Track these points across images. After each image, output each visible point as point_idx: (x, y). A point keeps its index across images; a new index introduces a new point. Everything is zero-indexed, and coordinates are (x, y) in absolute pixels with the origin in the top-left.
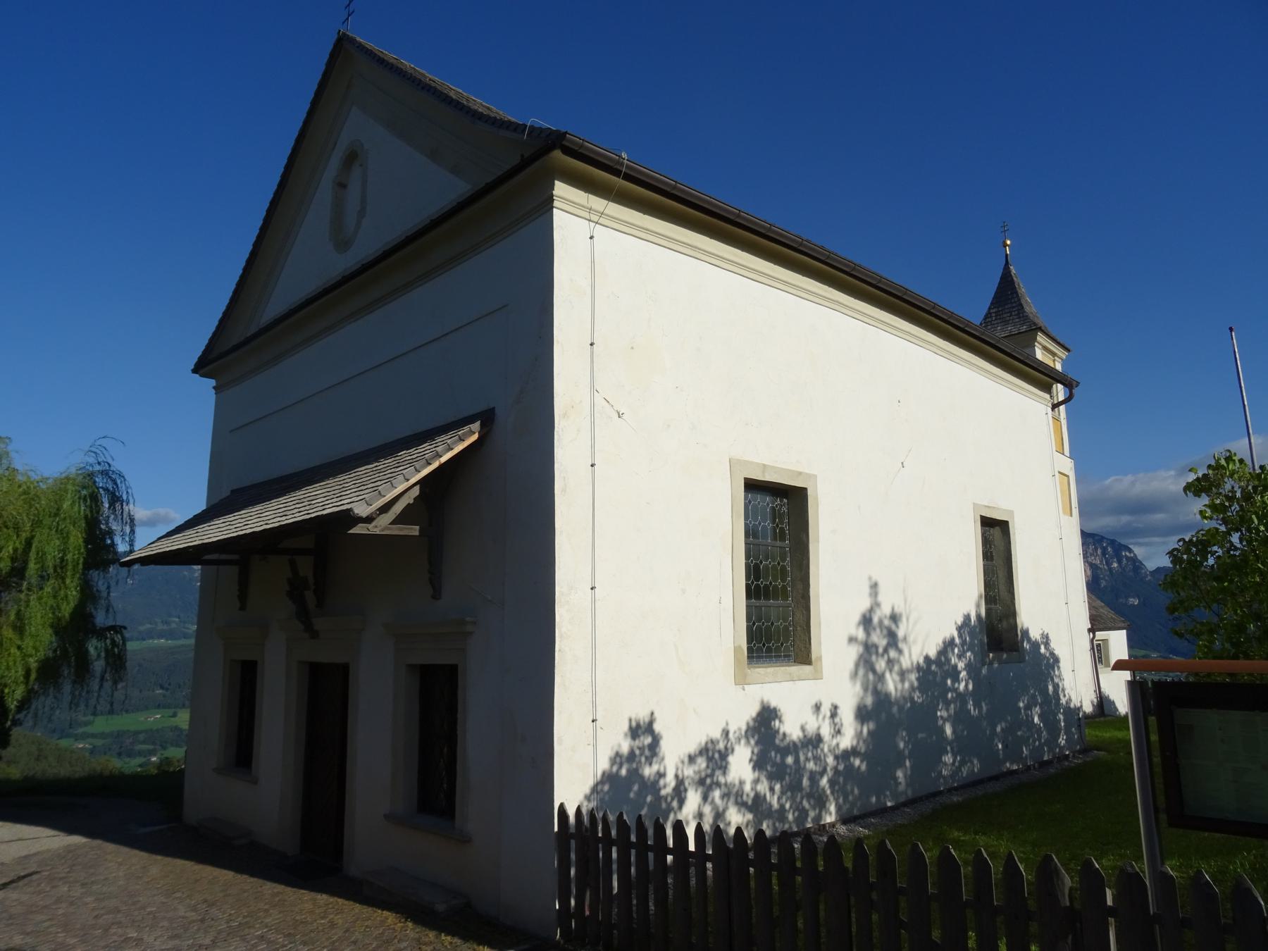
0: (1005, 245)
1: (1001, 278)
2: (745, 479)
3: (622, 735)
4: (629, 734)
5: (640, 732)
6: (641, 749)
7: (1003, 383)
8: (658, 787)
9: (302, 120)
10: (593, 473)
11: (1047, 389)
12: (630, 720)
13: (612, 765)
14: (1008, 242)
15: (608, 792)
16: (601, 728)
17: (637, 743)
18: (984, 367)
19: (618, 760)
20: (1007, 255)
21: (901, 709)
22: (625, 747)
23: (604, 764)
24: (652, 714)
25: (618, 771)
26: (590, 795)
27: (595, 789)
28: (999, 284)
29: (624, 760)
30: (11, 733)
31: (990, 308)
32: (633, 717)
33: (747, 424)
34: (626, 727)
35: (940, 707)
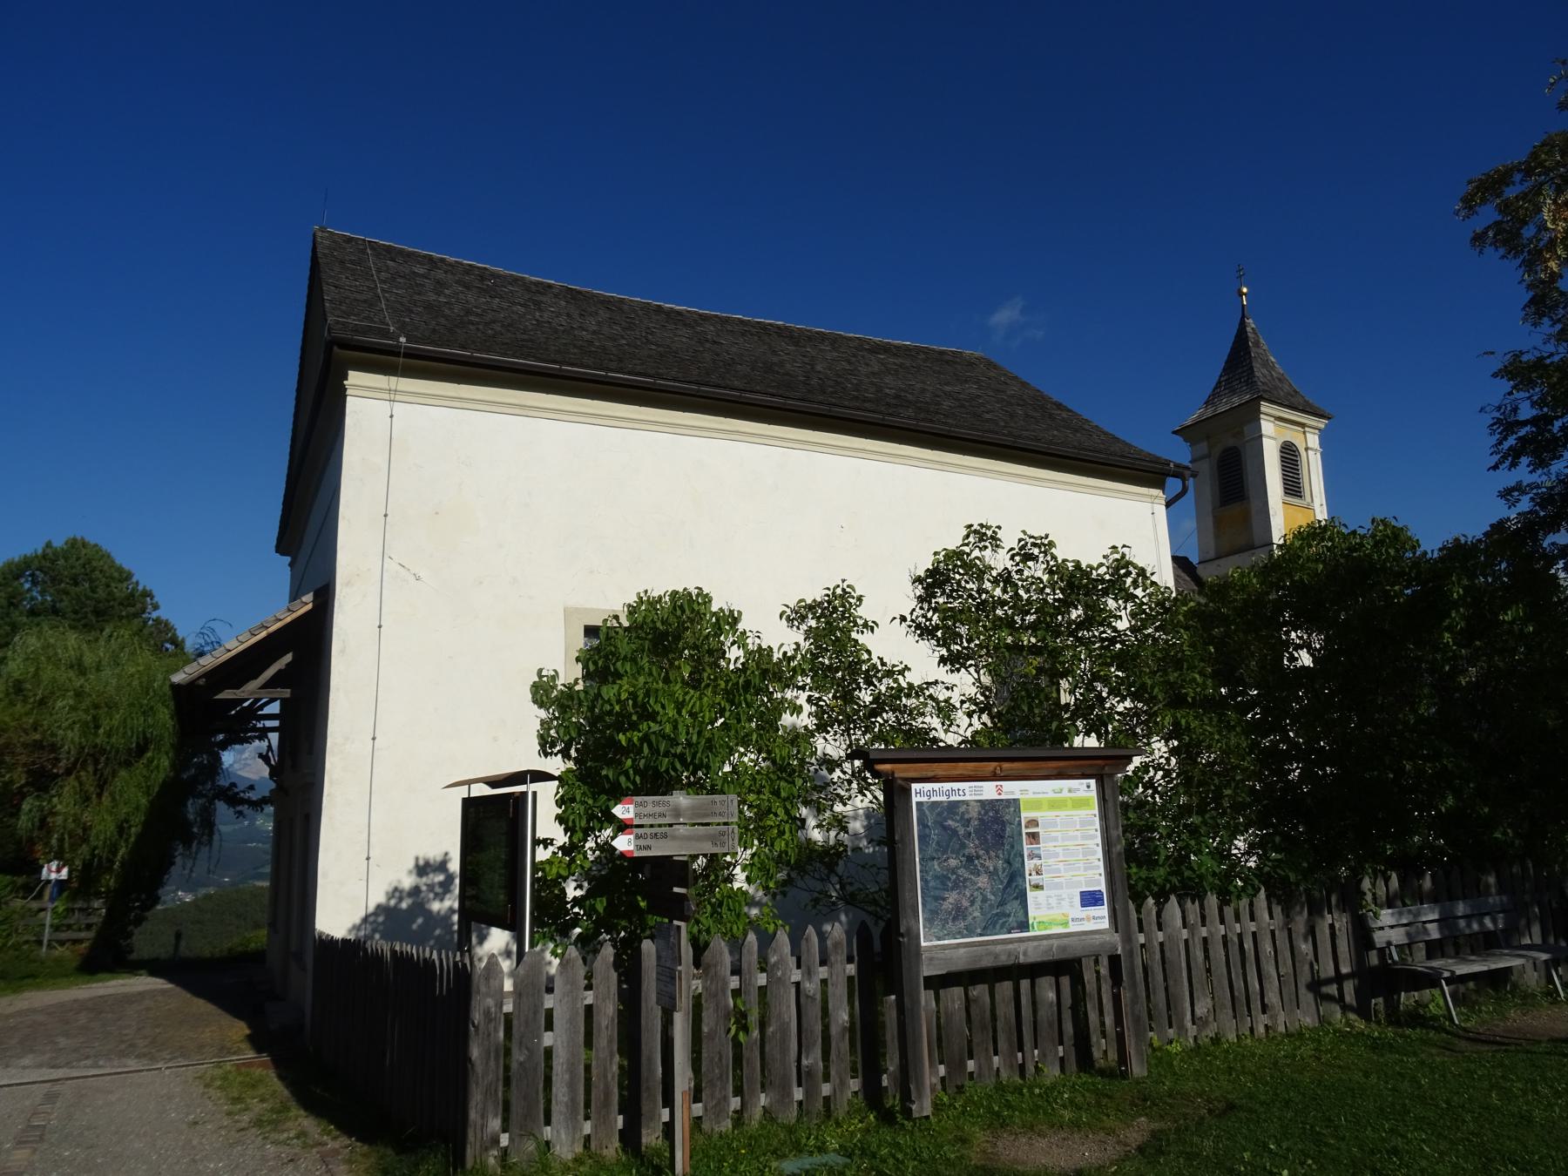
0: (1241, 294)
1: (1236, 336)
2: (585, 626)
3: (405, 872)
4: (415, 871)
5: (429, 870)
6: (431, 887)
7: (1059, 486)
8: (435, 914)
9: (309, 259)
10: (1154, 519)
11: (1159, 484)
12: (417, 859)
13: (389, 899)
14: (1245, 290)
15: (383, 923)
16: (378, 866)
17: (424, 879)
18: (1018, 472)
19: (397, 894)
20: (1243, 305)
21: (320, 937)
22: (408, 882)
23: (378, 897)
24: (446, 854)
25: (396, 904)
26: (360, 925)
27: (365, 920)
28: (1234, 343)
29: (404, 894)
30: (267, 794)
31: (1221, 376)
32: (421, 855)
33: (592, 572)
34: (411, 864)
35: (456, 918)
